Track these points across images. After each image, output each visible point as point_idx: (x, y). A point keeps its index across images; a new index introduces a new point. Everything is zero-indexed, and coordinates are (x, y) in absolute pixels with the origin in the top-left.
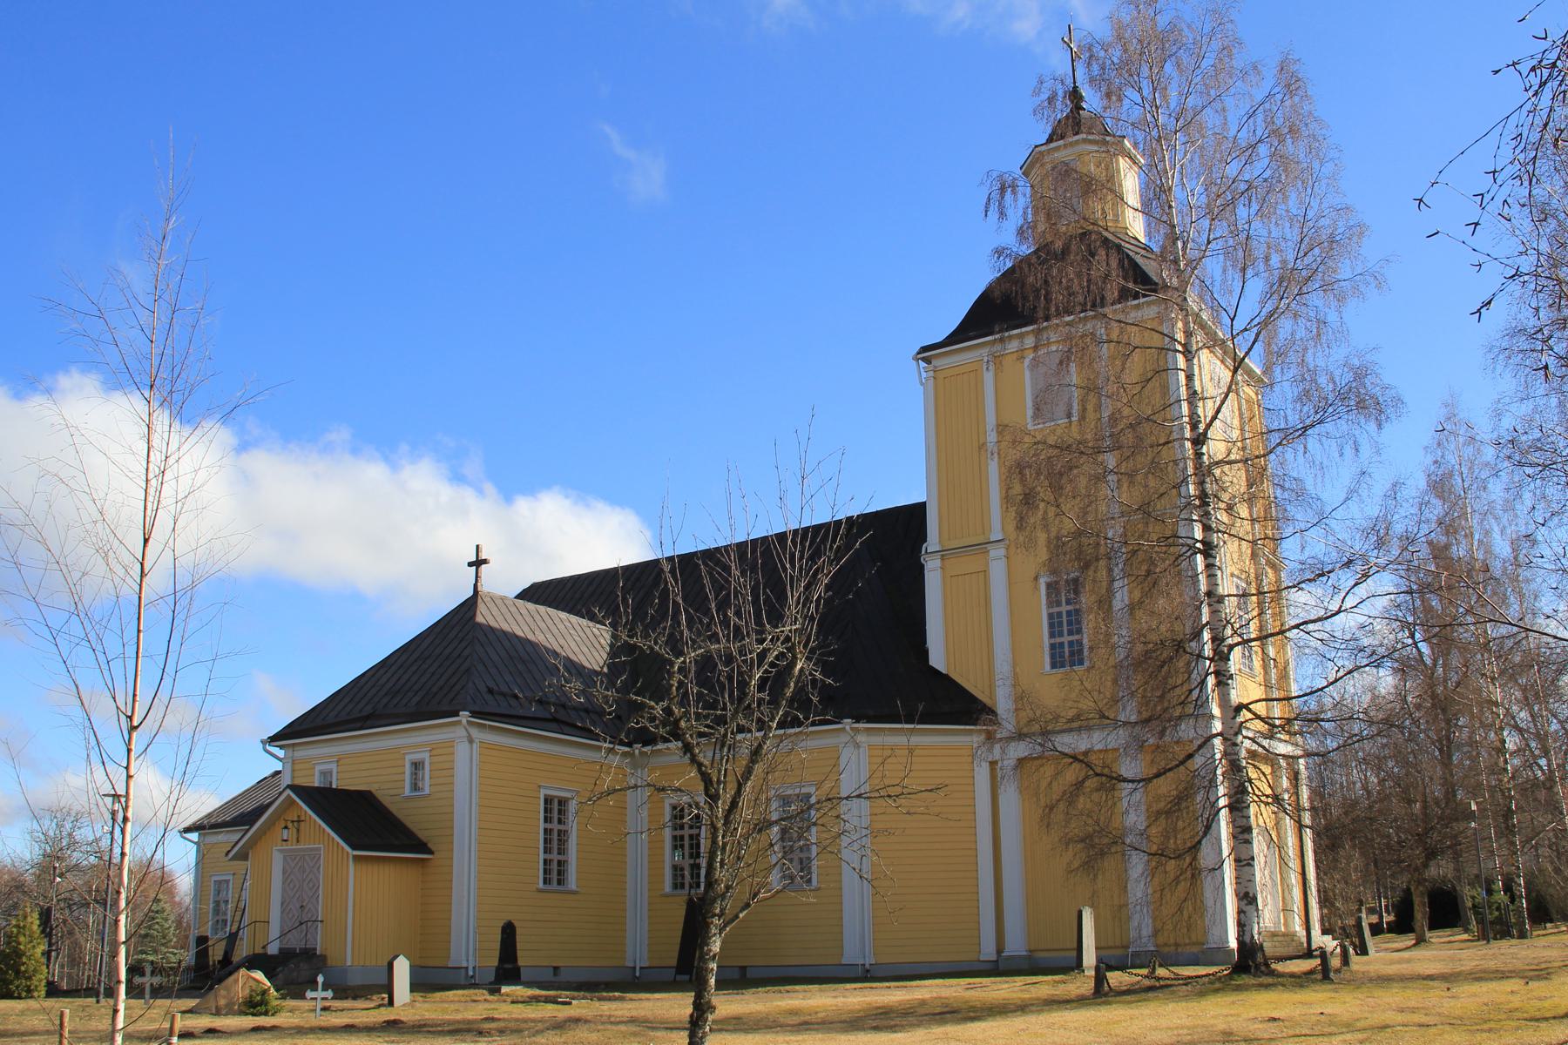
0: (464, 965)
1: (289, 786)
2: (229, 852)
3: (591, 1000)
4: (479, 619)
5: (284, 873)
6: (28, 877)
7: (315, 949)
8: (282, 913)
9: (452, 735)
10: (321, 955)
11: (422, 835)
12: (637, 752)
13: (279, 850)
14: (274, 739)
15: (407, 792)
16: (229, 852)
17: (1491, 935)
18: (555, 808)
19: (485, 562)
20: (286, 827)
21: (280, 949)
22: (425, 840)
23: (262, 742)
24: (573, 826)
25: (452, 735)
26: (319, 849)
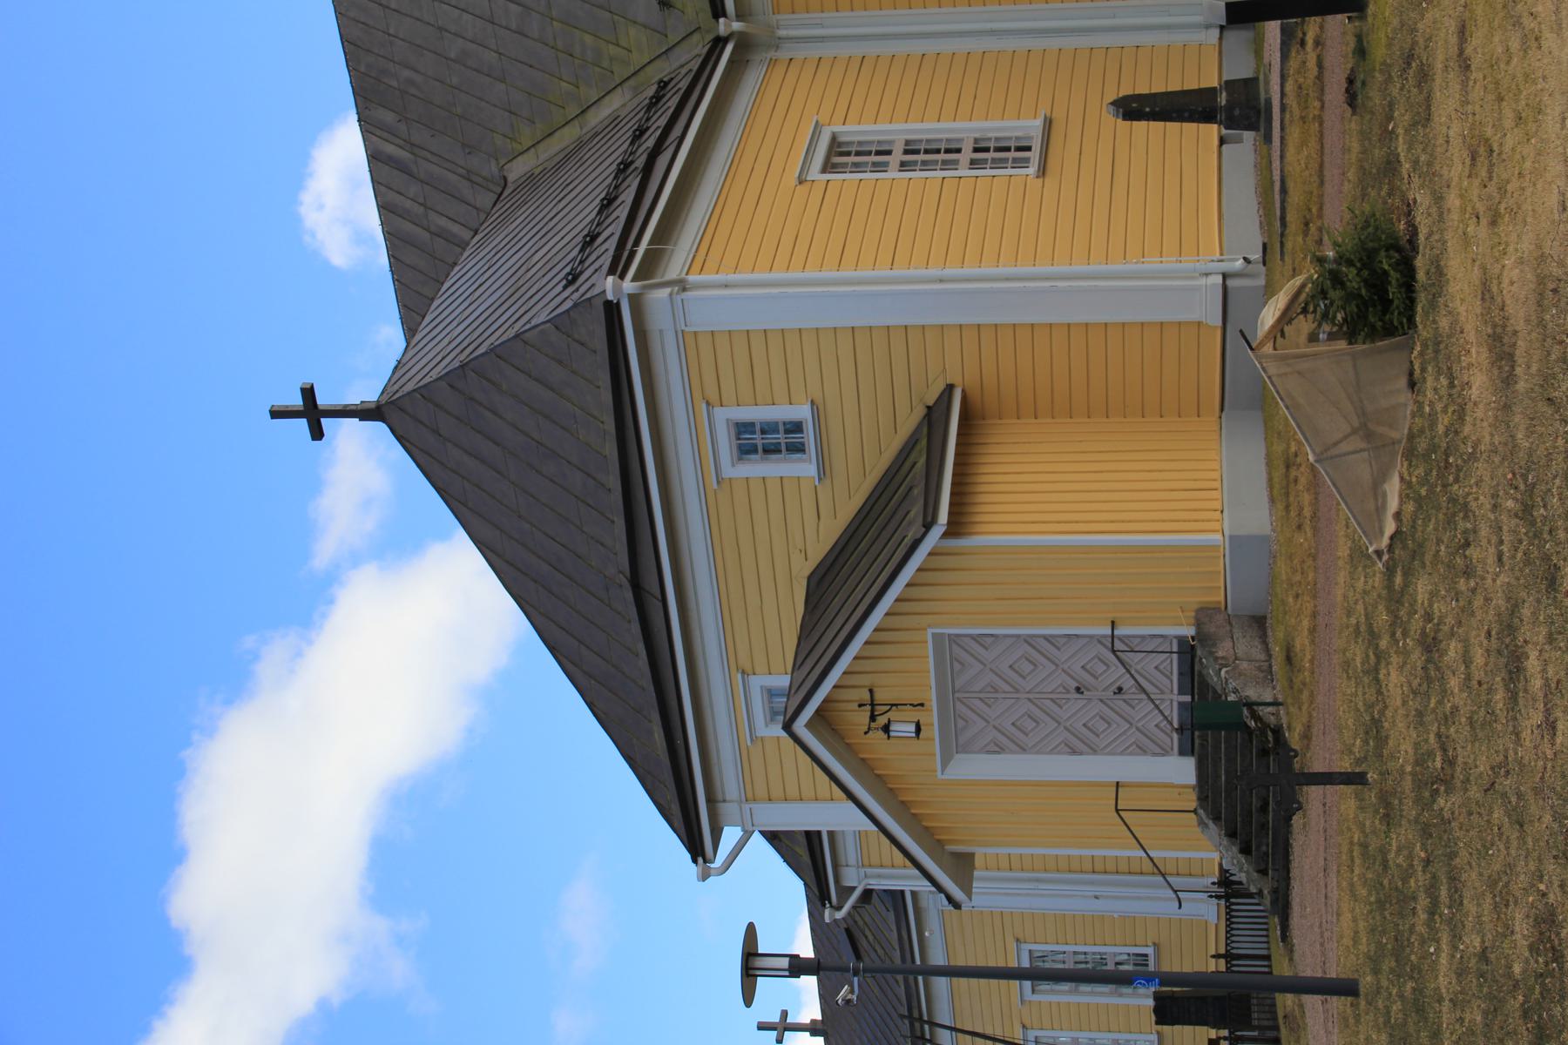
0: (1219, 279)
1: (788, 727)
2: (950, 899)
3: (1254, 145)
4: (822, 1038)
5: (1000, 749)
6: (1414, 295)
7: (1182, 640)
8: (1094, 751)
9: (670, 339)
10: (1199, 624)
11: (909, 421)
12: (736, 26)
13: (944, 766)
14: (697, 850)
15: (804, 468)
16: (950, 899)
17: (1440, 339)
18: (840, 155)
19: (308, 393)
20: (886, 729)
21: (1182, 753)
22: (920, 412)
23: (704, 876)
24: (966, 129)
25: (670, 339)
26: (934, 635)
